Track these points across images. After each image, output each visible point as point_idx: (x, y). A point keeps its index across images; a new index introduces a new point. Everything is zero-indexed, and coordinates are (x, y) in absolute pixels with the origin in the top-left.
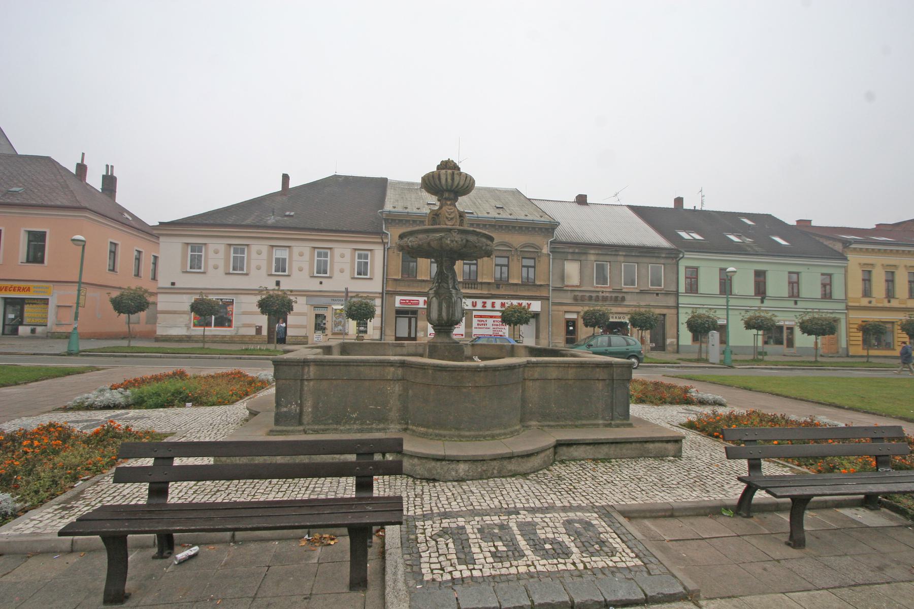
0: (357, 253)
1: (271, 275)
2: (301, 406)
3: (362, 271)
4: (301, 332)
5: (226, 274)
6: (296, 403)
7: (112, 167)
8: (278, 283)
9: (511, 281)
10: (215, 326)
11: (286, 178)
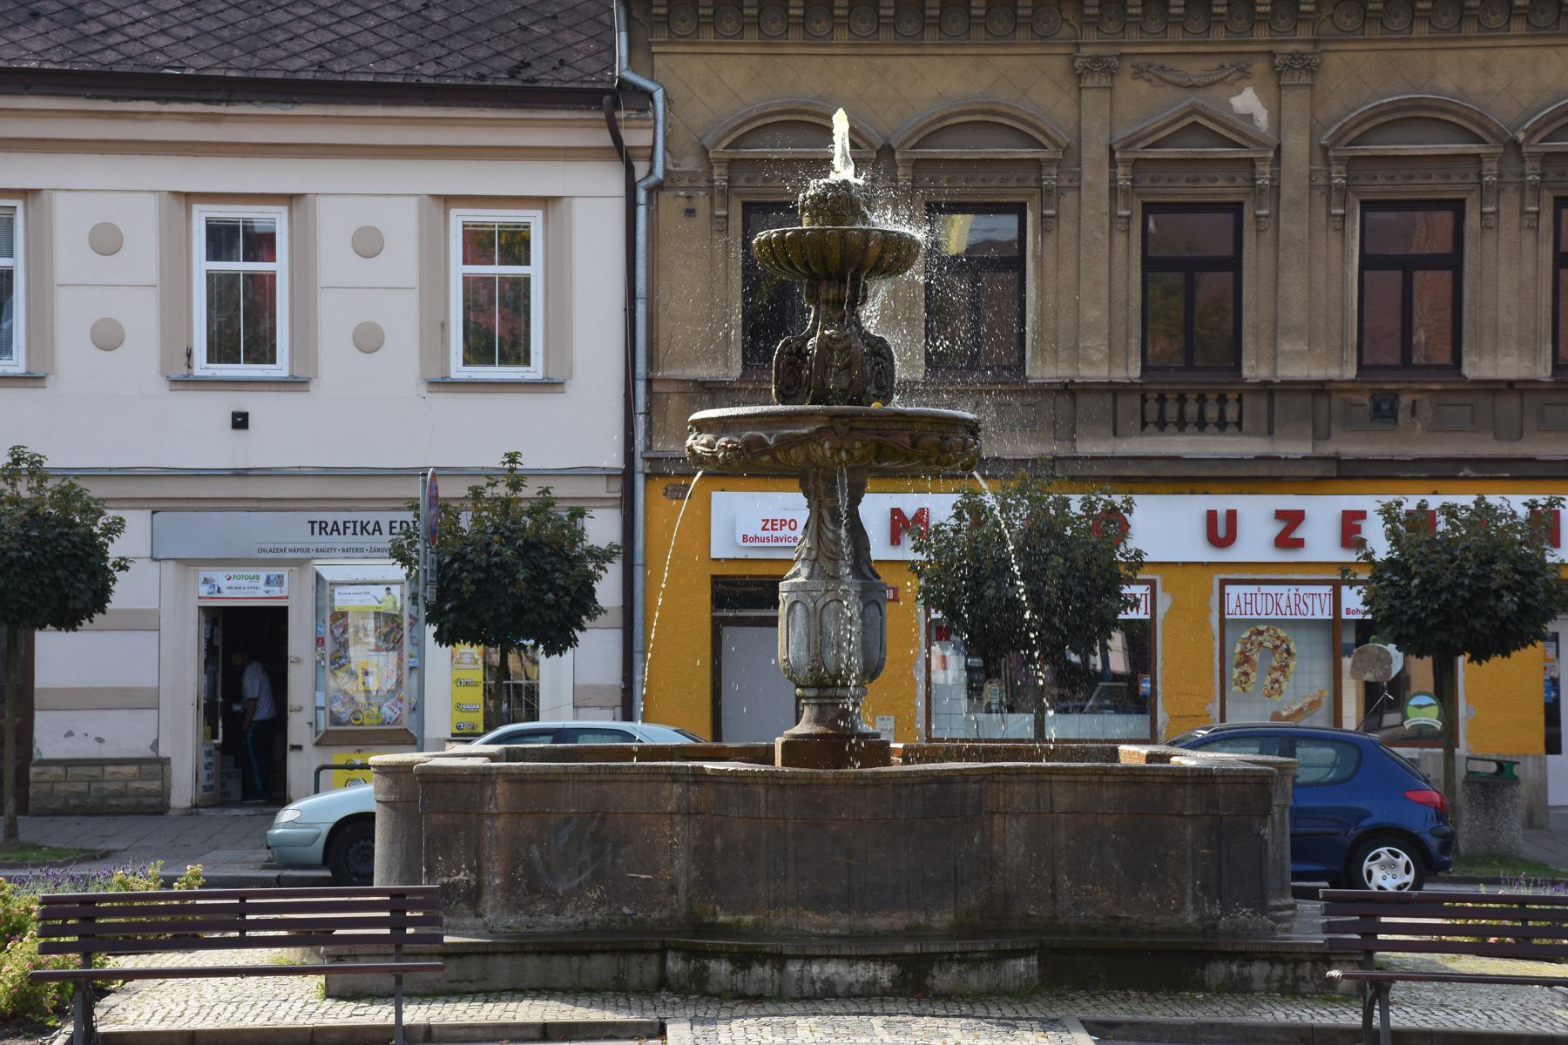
0: (459, 217)
1: (443, 384)
2: (478, 871)
3: (496, 330)
4: (124, 736)
6: (470, 867)
9: (1476, 367)
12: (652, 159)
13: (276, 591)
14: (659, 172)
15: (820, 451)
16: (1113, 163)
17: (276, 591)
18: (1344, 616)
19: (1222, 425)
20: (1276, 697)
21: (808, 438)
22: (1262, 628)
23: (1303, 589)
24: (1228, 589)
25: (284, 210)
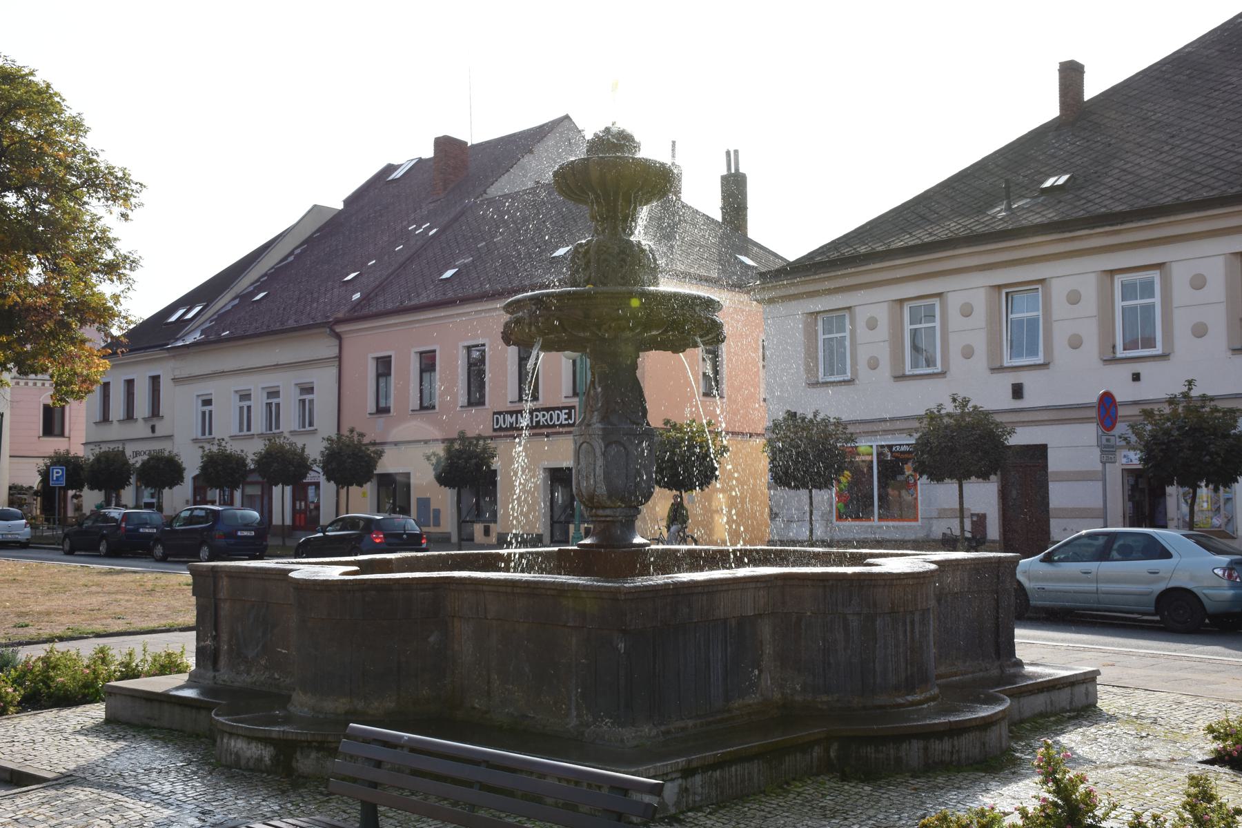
1: (1002, 369)
5: (994, 370)
7: (736, 152)
8: (1018, 391)
10: (880, 518)
11: (1071, 74)
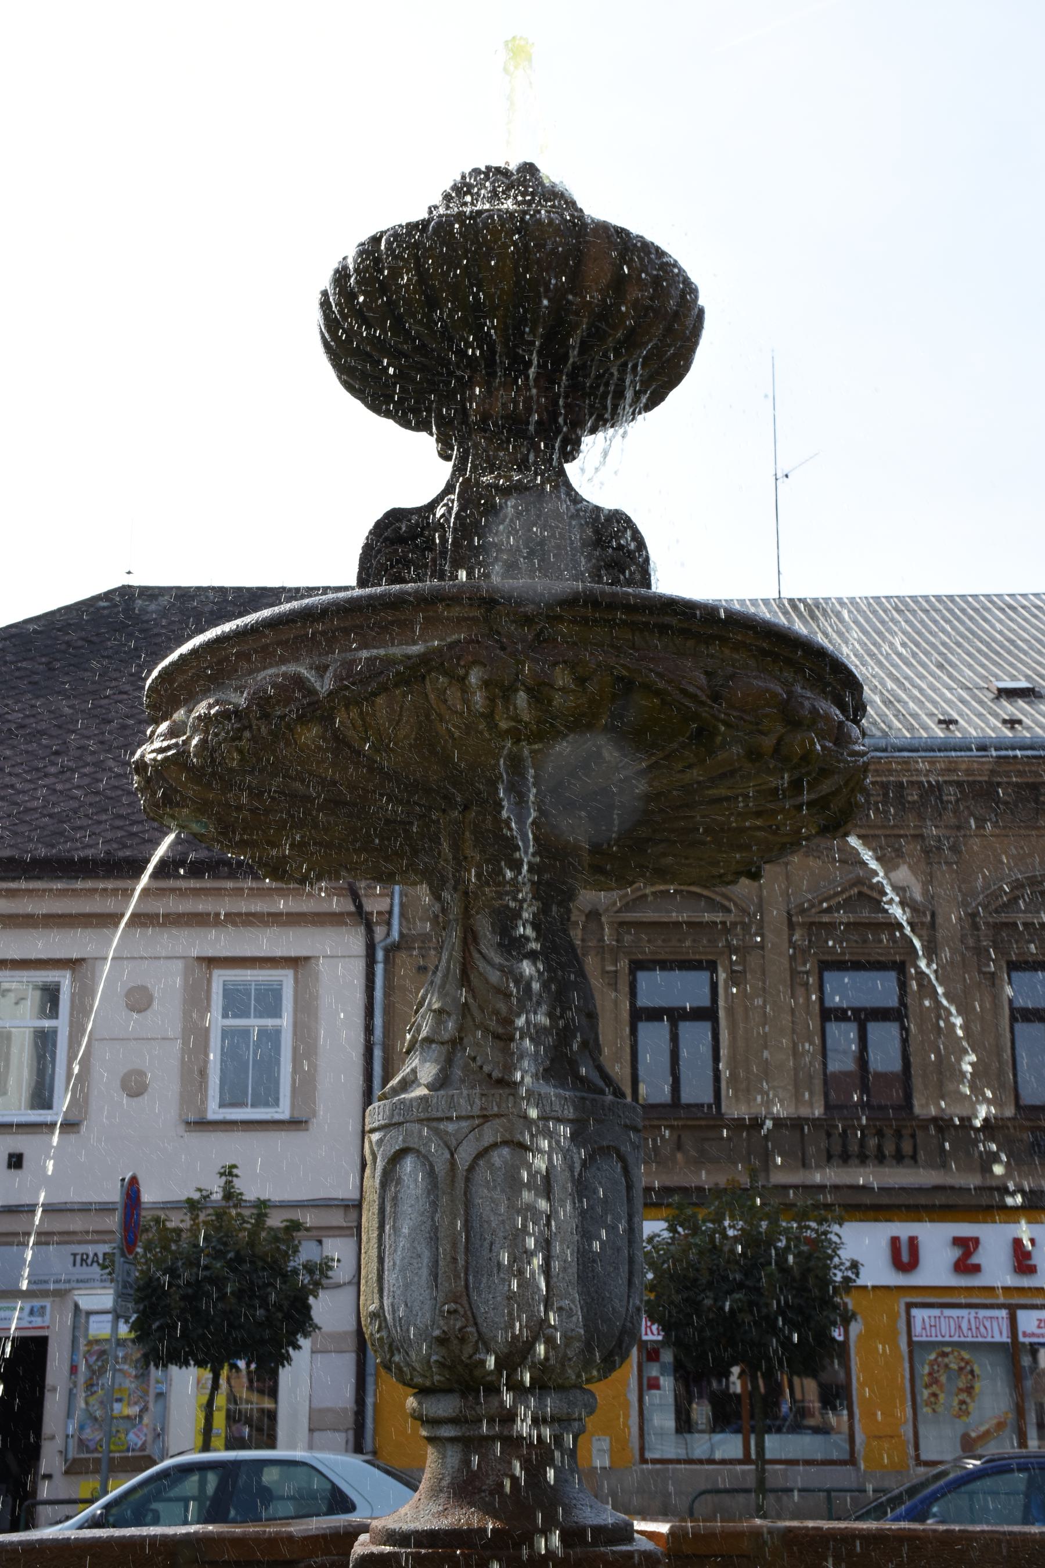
0: (220, 978)
1: (202, 1125)
12: (389, 924)
13: (38, 1321)
14: (395, 935)
15: (453, 695)
16: (791, 926)
17: (38, 1321)
18: (1021, 1339)
19: (899, 1158)
20: (964, 1419)
21: (415, 672)
22: (948, 1349)
23: (983, 1313)
24: (915, 1312)
25: (68, 974)
